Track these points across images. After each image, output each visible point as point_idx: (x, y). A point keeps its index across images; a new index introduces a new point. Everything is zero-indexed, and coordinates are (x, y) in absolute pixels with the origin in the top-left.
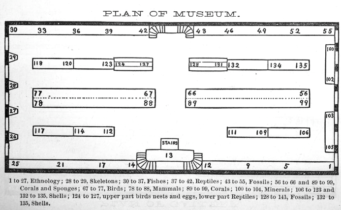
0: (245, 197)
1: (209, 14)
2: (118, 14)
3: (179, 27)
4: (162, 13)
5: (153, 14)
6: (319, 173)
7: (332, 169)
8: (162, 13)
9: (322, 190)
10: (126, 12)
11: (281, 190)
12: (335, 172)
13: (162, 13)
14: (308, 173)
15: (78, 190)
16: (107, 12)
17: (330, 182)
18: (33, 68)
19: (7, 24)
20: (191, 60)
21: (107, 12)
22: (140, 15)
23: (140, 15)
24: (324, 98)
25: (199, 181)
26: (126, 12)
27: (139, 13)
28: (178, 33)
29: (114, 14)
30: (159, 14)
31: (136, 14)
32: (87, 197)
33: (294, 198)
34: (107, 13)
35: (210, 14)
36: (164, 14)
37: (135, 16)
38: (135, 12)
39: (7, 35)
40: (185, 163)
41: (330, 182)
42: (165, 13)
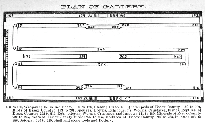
0: (105, 120)
1: (128, 6)
2: (70, 7)
3: (108, 15)
4: (96, 6)
5: (91, 7)
6: (106, 101)
7: (200, 99)
8: (96, 6)
9: (172, 114)
10: (75, 6)
11: (167, 114)
12: (202, 101)
13: (96, 6)
14: (31, 101)
15: (136, 115)
16: (64, 6)
17: (199, 107)
18: (188, 66)
19: (5, 13)
20: (186, 50)
21: (64, 6)
22: (83, 8)
23: (83, 8)
24: (195, 57)
25: (184, 110)
26: (75, 6)
27: (83, 6)
28: (108, 17)
29: (67, 7)
30: (95, 7)
31: (81, 7)
32: (45, 121)
33: (101, 121)
34: (63, 7)
35: (129, 7)
36: (97, 7)
37: (80, 8)
38: (80, 6)
39: (5, 20)
40: (110, 97)
41: (199, 107)
42: (98, 6)
